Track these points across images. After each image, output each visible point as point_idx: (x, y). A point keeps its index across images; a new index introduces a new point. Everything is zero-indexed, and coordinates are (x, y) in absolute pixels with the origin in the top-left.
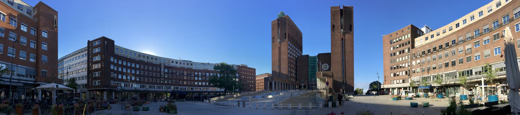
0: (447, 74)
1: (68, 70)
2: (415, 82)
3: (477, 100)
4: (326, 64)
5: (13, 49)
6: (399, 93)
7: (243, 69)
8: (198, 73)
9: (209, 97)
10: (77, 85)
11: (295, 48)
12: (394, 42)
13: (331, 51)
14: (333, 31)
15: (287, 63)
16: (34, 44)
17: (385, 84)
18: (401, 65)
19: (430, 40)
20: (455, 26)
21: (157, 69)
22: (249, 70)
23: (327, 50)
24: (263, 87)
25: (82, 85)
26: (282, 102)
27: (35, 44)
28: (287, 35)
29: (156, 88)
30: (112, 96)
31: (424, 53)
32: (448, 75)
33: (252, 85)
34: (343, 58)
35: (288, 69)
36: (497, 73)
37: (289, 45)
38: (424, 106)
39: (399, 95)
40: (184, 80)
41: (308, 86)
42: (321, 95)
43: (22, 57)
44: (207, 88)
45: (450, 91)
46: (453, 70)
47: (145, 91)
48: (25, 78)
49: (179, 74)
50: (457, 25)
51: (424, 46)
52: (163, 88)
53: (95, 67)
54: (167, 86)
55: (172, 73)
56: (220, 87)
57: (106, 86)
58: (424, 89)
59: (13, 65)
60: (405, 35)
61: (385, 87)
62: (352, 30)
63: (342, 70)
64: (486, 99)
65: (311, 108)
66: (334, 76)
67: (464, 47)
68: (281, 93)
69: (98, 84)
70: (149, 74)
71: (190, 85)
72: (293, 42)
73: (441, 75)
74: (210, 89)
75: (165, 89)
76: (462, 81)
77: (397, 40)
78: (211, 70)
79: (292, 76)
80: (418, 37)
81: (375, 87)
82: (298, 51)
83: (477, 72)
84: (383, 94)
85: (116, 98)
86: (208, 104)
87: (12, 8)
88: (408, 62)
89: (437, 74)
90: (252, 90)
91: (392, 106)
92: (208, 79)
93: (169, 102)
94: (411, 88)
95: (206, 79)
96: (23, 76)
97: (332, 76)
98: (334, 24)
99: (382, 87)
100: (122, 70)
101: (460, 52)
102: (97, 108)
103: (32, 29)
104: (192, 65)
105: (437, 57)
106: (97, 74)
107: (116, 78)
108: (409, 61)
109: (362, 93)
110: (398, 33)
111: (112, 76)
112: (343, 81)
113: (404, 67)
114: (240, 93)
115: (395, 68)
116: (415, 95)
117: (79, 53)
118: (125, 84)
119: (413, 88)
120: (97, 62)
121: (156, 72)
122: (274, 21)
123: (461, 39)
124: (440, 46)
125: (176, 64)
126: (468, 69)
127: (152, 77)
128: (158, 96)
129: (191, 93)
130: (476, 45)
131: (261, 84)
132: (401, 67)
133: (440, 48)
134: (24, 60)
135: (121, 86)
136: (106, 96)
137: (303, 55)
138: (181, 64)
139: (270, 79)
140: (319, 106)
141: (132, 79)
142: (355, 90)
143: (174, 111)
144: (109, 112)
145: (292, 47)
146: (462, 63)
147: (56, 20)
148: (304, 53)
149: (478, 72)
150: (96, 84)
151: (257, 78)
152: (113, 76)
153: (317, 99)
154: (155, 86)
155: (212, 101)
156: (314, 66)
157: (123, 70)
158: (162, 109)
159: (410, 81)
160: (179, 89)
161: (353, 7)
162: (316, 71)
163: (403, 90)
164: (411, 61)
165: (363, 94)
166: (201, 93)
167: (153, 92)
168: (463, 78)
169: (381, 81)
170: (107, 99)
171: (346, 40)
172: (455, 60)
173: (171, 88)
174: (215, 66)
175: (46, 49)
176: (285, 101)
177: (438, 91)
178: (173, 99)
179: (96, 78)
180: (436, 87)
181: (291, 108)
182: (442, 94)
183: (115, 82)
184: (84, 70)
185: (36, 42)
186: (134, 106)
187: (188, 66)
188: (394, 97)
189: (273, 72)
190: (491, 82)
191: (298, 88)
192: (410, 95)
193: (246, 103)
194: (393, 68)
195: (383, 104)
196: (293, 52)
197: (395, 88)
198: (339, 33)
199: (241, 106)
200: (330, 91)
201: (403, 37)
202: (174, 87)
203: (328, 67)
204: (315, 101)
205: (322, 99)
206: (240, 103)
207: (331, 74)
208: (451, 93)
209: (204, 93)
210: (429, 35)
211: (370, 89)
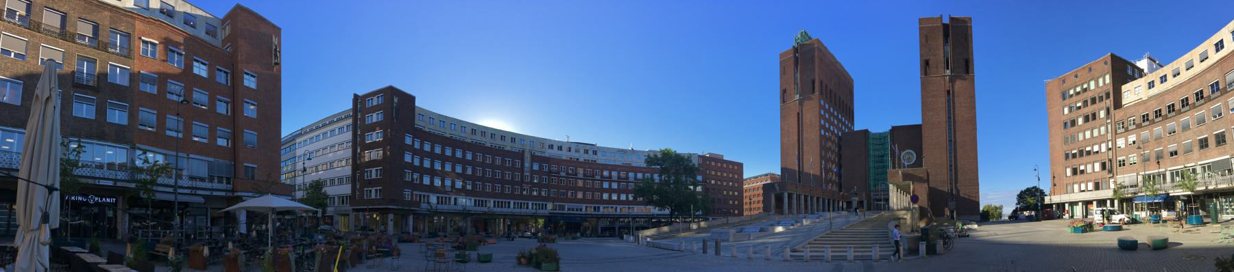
0: (1206, 165)
1: (306, 162)
2: (1125, 187)
4: (910, 151)
5: (176, 118)
6: (1087, 213)
7: (713, 164)
8: (610, 173)
9: (634, 229)
10: (326, 196)
11: (829, 107)
12: (1071, 96)
13: (923, 121)
14: (926, 75)
15: (818, 150)
16: (225, 104)
17: (1053, 193)
18: (1088, 149)
19: (1159, 88)
20: (1214, 48)
21: (514, 164)
23: (913, 117)
24: (761, 205)
25: (339, 197)
26: (809, 244)
27: (227, 106)
29: (512, 208)
30: (407, 224)
31: (1145, 118)
32: (1209, 167)
34: (950, 136)
35: (821, 163)
37: (821, 107)
39: (1088, 221)
40: (576, 189)
41: (868, 201)
43: (197, 137)
44: (629, 208)
45: (1218, 207)
46: (1221, 155)
47: (485, 213)
48: (208, 185)
50: (1216, 45)
51: (1145, 102)
52: (527, 208)
54: (538, 202)
55: (550, 172)
56: (661, 205)
59: (180, 154)
61: (1055, 200)
65: (878, 257)
66: (930, 178)
68: (804, 221)
70: (494, 174)
71: (591, 202)
72: (826, 97)
73: (1191, 168)
75: (532, 208)
77: (1078, 89)
78: (639, 165)
79: (831, 179)
80: (1129, 82)
81: (1031, 201)
82: (847, 123)
85: (415, 229)
87: (165, 23)
88: (1108, 141)
89: (1183, 166)
91: (1071, 247)
92: (631, 186)
93: (542, 240)
96: (202, 180)
98: (927, 58)
99: (1047, 200)
100: (432, 164)
102: (369, 253)
103: (221, 71)
104: (596, 154)
105: (1178, 125)
106: (374, 173)
107: (418, 182)
108: (1110, 138)
109: (1000, 215)
111: (408, 178)
112: (952, 190)
113: (1097, 152)
114: (706, 220)
115: (1074, 156)
116: (1126, 219)
117: (332, 123)
118: (438, 198)
119: (1122, 201)
120: (374, 146)
121: (513, 169)
124: (1183, 101)
125: (560, 152)
127: (503, 182)
128: (517, 225)
131: (756, 199)
132: (1089, 153)
133: (1183, 106)
134: (204, 143)
135: (428, 203)
137: (855, 130)
138: (570, 151)
139: (777, 188)
142: (981, 209)
144: (396, 262)
147: (276, 47)
148: (858, 126)
150: (370, 196)
154: (509, 203)
156: (882, 156)
158: (522, 260)
159: (1112, 186)
161: (970, 19)
162: (886, 167)
163: (1097, 207)
164: (1114, 138)
165: (1003, 219)
166: (617, 218)
167: (506, 215)
169: (1045, 186)
171: (956, 94)
172: (1224, 130)
173: (546, 208)
174: (649, 156)
175: (255, 116)
176: (815, 240)
178: (550, 232)
179: (371, 183)
180: (1181, 198)
181: (830, 258)
184: (344, 163)
185: (229, 100)
187: (586, 157)
188: (1075, 226)
189: (783, 169)
191: (845, 206)
192: (1116, 218)
193: (722, 244)
194: (1070, 156)
195: (1051, 243)
196: (832, 124)
197: (1076, 203)
198: (939, 78)
199: (711, 251)
200: (923, 213)
201: (1092, 84)
203: (915, 159)
206: (708, 243)
207: (924, 175)
208: (1222, 211)
210: (1155, 76)
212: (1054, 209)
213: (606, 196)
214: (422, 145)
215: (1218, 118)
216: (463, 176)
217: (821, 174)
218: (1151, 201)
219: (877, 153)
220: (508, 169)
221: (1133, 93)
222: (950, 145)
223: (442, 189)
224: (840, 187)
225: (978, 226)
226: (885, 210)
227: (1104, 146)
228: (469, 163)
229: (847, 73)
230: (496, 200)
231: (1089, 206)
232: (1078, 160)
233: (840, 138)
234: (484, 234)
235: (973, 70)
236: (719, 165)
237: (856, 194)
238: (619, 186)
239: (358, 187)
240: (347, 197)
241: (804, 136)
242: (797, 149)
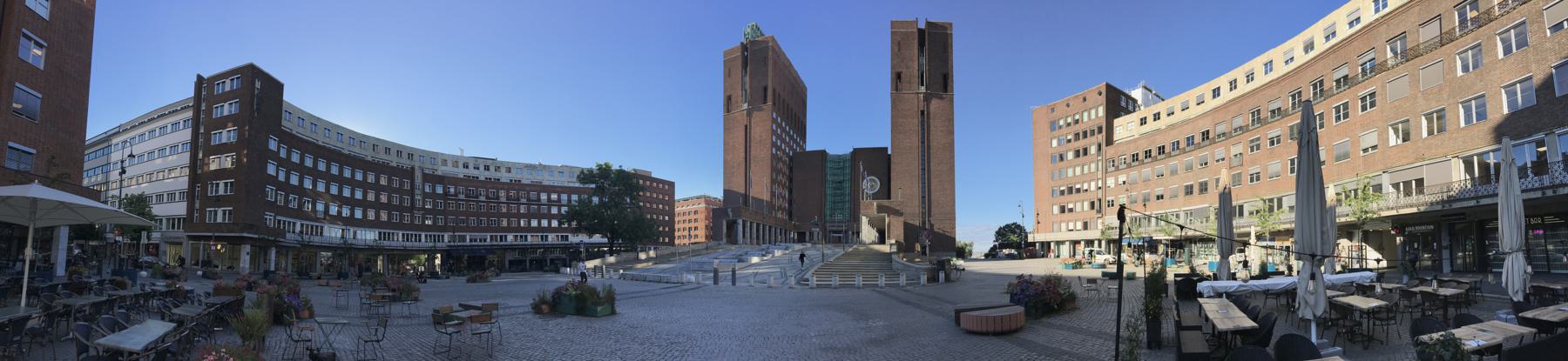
4: (873, 178)
8: (559, 196)
12: (1060, 127)
15: (768, 171)
18: (1078, 186)
19: (1151, 125)
21: (402, 184)
23: (879, 136)
25: (168, 220)
31: (1135, 157)
32: (1191, 213)
37: (774, 121)
51: (1135, 141)
57: (250, 228)
62: (949, 88)
77: (1069, 120)
78: (552, 184)
81: (1014, 238)
84: (1033, 255)
88: (1098, 179)
94: (1103, 243)
95: (539, 209)
99: (1030, 239)
100: (301, 181)
101: (1218, 161)
108: (1100, 176)
112: (924, 223)
113: (1086, 190)
115: (1062, 193)
122: (732, 51)
123: (1221, 129)
132: (1078, 191)
136: (248, 257)
137: (807, 150)
141: (331, 213)
148: (811, 146)
152: (271, 198)
154: (420, 236)
156: (840, 182)
157: (289, 178)
158: (544, 307)
161: (951, 24)
169: (1029, 226)
170: (250, 268)
171: (932, 116)
173: (506, 240)
174: (582, 172)
179: (219, 201)
183: (279, 218)
187: (488, 174)
189: (726, 192)
196: (783, 141)
197: (1063, 242)
201: (1086, 114)
211: (996, 243)
214: (289, 153)
219: (836, 178)
227: (1093, 184)
228: (383, 189)
229: (802, 82)
231: (1077, 246)
232: (1067, 197)
235: (952, 87)
239: (197, 206)
240: (179, 219)
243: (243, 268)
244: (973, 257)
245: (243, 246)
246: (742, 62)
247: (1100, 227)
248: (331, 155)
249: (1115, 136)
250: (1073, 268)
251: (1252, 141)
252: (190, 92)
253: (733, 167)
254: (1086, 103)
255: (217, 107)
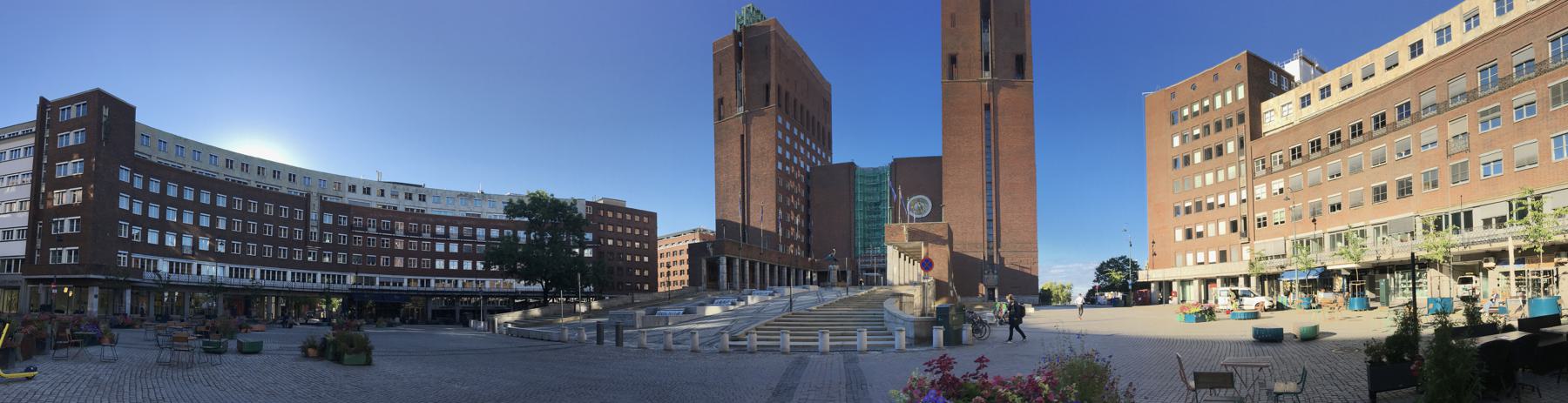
3: (1491, 314)
4: (923, 197)
7: (610, 214)
8: (447, 230)
9: (485, 312)
12: (1186, 118)
13: (944, 152)
15: (773, 193)
17: (1153, 266)
18: (1210, 200)
19: (1318, 106)
21: (293, 213)
22: (641, 219)
24: (686, 277)
26: (757, 329)
28: (773, 91)
29: (289, 280)
30: (122, 301)
31: (1296, 153)
32: (1385, 228)
33: (642, 273)
35: (777, 212)
36: (1560, 224)
38: (1301, 336)
40: (394, 253)
42: (901, 303)
44: (477, 282)
45: (1392, 286)
47: (246, 288)
49: (375, 230)
52: (314, 281)
53: (64, 197)
56: (529, 277)
57: (97, 268)
58: (1302, 282)
60: (1226, 89)
61: (1154, 276)
63: (985, 220)
64: (1520, 309)
65: (865, 348)
67: (1443, 129)
68: (749, 297)
69: (69, 259)
70: (261, 228)
73: (1359, 229)
74: (488, 284)
75: (323, 282)
76: (1437, 248)
77: (1196, 108)
78: (493, 217)
79: (792, 237)
81: (1117, 276)
83: (1491, 219)
84: (1147, 301)
85: (134, 310)
86: (484, 334)
88: (1241, 189)
89: (1346, 227)
90: (642, 287)
94: (1253, 280)
95: (474, 248)
97: (946, 238)
98: (953, 52)
99: (1142, 277)
104: (424, 200)
105: (1345, 164)
106: (67, 225)
110: (1197, 84)
111: (124, 235)
113: (1223, 205)
115: (1188, 210)
116: (1267, 304)
118: (171, 264)
121: (290, 222)
123: (1428, 99)
124: (1354, 128)
125: (366, 197)
126: (1457, 209)
127: (276, 241)
128: (297, 307)
129: (421, 298)
130: (1485, 123)
131: (678, 268)
132: (1211, 206)
135: (156, 271)
136: (96, 301)
137: (834, 162)
138: (382, 195)
139: (711, 250)
140: (893, 340)
142: (1040, 287)
143: (362, 358)
145: (790, 133)
146: (1435, 185)
148: (839, 157)
149: (1494, 220)
150: (60, 260)
151: (662, 248)
153: (886, 315)
154: (285, 273)
155: (499, 325)
156: (877, 204)
158: (311, 351)
160: (419, 281)
162: (884, 220)
163: (1222, 286)
168: (1438, 239)
170: (99, 312)
171: (1000, 111)
172: (1410, 175)
173: (344, 282)
174: (510, 202)
177: (1348, 287)
179: (63, 240)
180: (1344, 273)
182: (1363, 296)
184: (16, 207)
186: (207, 337)
187: (409, 204)
189: (719, 223)
190: (1539, 253)
191: (815, 279)
192: (1250, 304)
194: (1182, 211)
197: (1189, 282)
199: (609, 341)
200: (940, 289)
201: (1218, 99)
202: (357, 278)
204: (879, 324)
205: (906, 316)
207: (944, 234)
209: (466, 296)
210: (1312, 88)
211: (1097, 284)
212: (1152, 290)
213: (440, 264)
214: (146, 183)
215: (1404, 156)
216: (212, 232)
217: (778, 229)
218: (1303, 278)
220: (284, 222)
221: (1279, 113)
222: (989, 189)
223: (178, 251)
224: (808, 249)
225: (1035, 310)
226: (878, 284)
228: (222, 212)
230: (266, 269)
232: (1194, 215)
233: (808, 176)
234: (245, 318)
236: (619, 216)
237: (835, 260)
238: (460, 248)
240: (17, 261)
241: (751, 171)
242: (740, 192)
243: (91, 312)
244: (1072, 303)
245: (90, 288)
246: (736, 55)
247: (1247, 256)
248: (199, 181)
249: (1263, 125)
250: (1198, 320)
251: (1484, 114)
252: (31, 115)
253: (727, 191)
254: (1218, 82)
255: (63, 136)
